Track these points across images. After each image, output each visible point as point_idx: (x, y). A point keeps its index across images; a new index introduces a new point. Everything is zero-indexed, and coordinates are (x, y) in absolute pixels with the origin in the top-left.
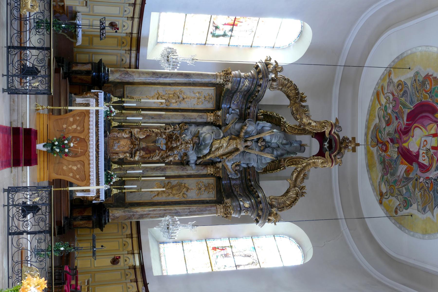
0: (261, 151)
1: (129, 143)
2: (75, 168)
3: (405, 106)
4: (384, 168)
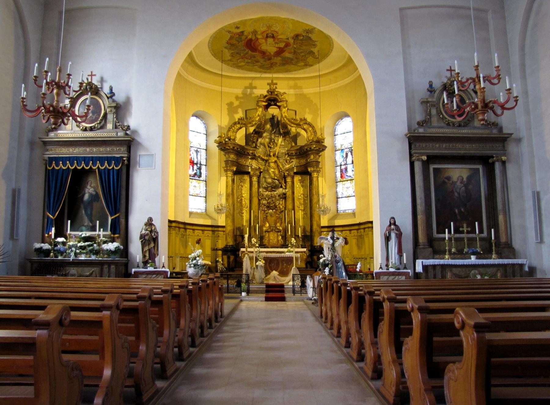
0: (277, 145)
1: (271, 233)
2: (285, 265)
3: (247, 53)
4: (288, 64)
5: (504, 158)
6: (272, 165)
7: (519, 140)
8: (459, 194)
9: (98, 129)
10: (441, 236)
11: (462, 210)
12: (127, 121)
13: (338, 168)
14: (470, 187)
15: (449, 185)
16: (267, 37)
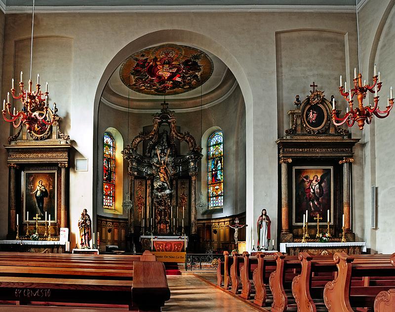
5: (351, 160)
6: (162, 171)
7: (363, 145)
8: (314, 190)
9: (46, 139)
10: (299, 224)
11: (316, 203)
12: (67, 133)
13: (210, 174)
15: (306, 182)
16: (164, 63)
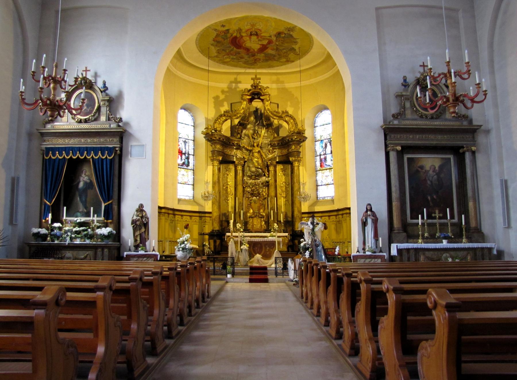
0: (260, 136)
1: (255, 218)
2: (268, 248)
3: (232, 50)
5: (473, 148)
6: (256, 154)
7: (488, 132)
8: (431, 182)
10: (415, 221)
11: (435, 197)
12: (120, 114)
13: (318, 158)
14: (442, 175)
15: (422, 173)
16: (251, 35)
